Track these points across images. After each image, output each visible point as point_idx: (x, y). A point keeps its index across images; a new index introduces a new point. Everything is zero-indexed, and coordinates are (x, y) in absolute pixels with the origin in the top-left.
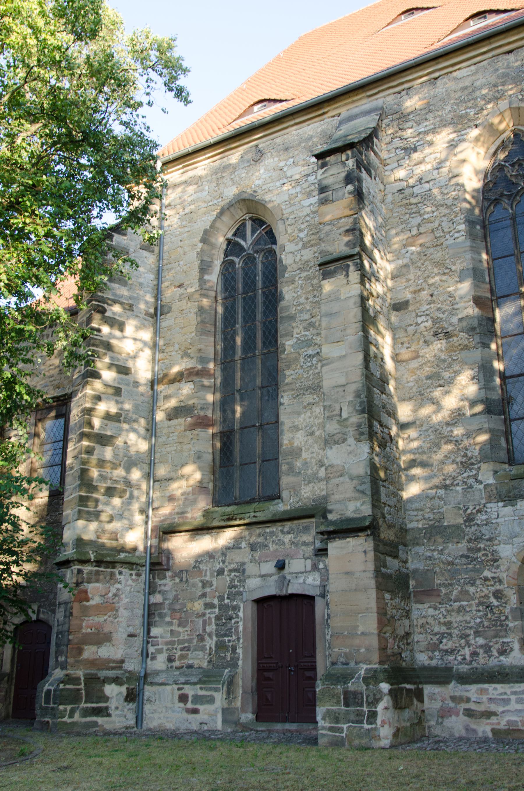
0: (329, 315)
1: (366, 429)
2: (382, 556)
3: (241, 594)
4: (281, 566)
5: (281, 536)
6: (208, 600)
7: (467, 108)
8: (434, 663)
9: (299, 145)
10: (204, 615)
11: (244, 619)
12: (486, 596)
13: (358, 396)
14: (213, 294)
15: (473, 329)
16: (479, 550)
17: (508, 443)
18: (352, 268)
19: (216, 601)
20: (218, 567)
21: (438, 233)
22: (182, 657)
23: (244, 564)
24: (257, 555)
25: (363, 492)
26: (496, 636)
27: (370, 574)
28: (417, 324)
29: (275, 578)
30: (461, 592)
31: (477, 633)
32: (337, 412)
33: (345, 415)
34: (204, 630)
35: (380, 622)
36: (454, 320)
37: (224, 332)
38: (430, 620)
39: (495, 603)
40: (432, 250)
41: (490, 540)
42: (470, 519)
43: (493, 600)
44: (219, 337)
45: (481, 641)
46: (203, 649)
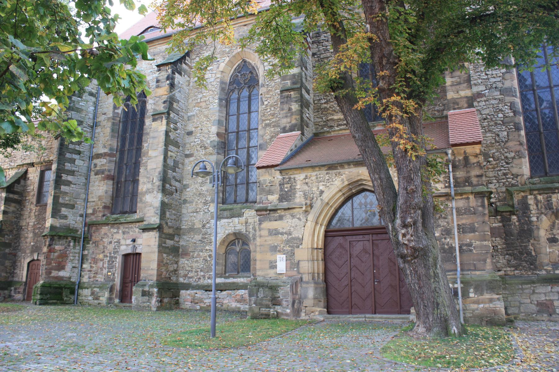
0: (154, 138)
1: (161, 188)
2: (163, 240)
3: (118, 252)
4: (134, 241)
5: (135, 229)
6: (105, 254)
7: (226, 48)
8: (185, 282)
9: (159, 54)
10: (103, 260)
11: (118, 262)
12: (206, 257)
13: (160, 174)
14: (119, 119)
15: (215, 146)
16: (206, 238)
17: (223, 195)
18: (164, 118)
19: (108, 255)
20: (110, 240)
21: (208, 103)
22: (94, 277)
23: (120, 240)
24: (125, 236)
25: (157, 214)
26: (207, 272)
27: (157, 246)
28: (195, 142)
29: (131, 246)
30: (197, 255)
31: (201, 271)
32: (151, 180)
33: (154, 181)
34: (103, 266)
35: (159, 265)
36: (209, 142)
37: (122, 136)
38: (186, 265)
39: (209, 259)
40: (204, 110)
41: (210, 234)
42: (204, 226)
43: (208, 258)
44: (119, 140)
45: (202, 273)
46: (102, 274)
